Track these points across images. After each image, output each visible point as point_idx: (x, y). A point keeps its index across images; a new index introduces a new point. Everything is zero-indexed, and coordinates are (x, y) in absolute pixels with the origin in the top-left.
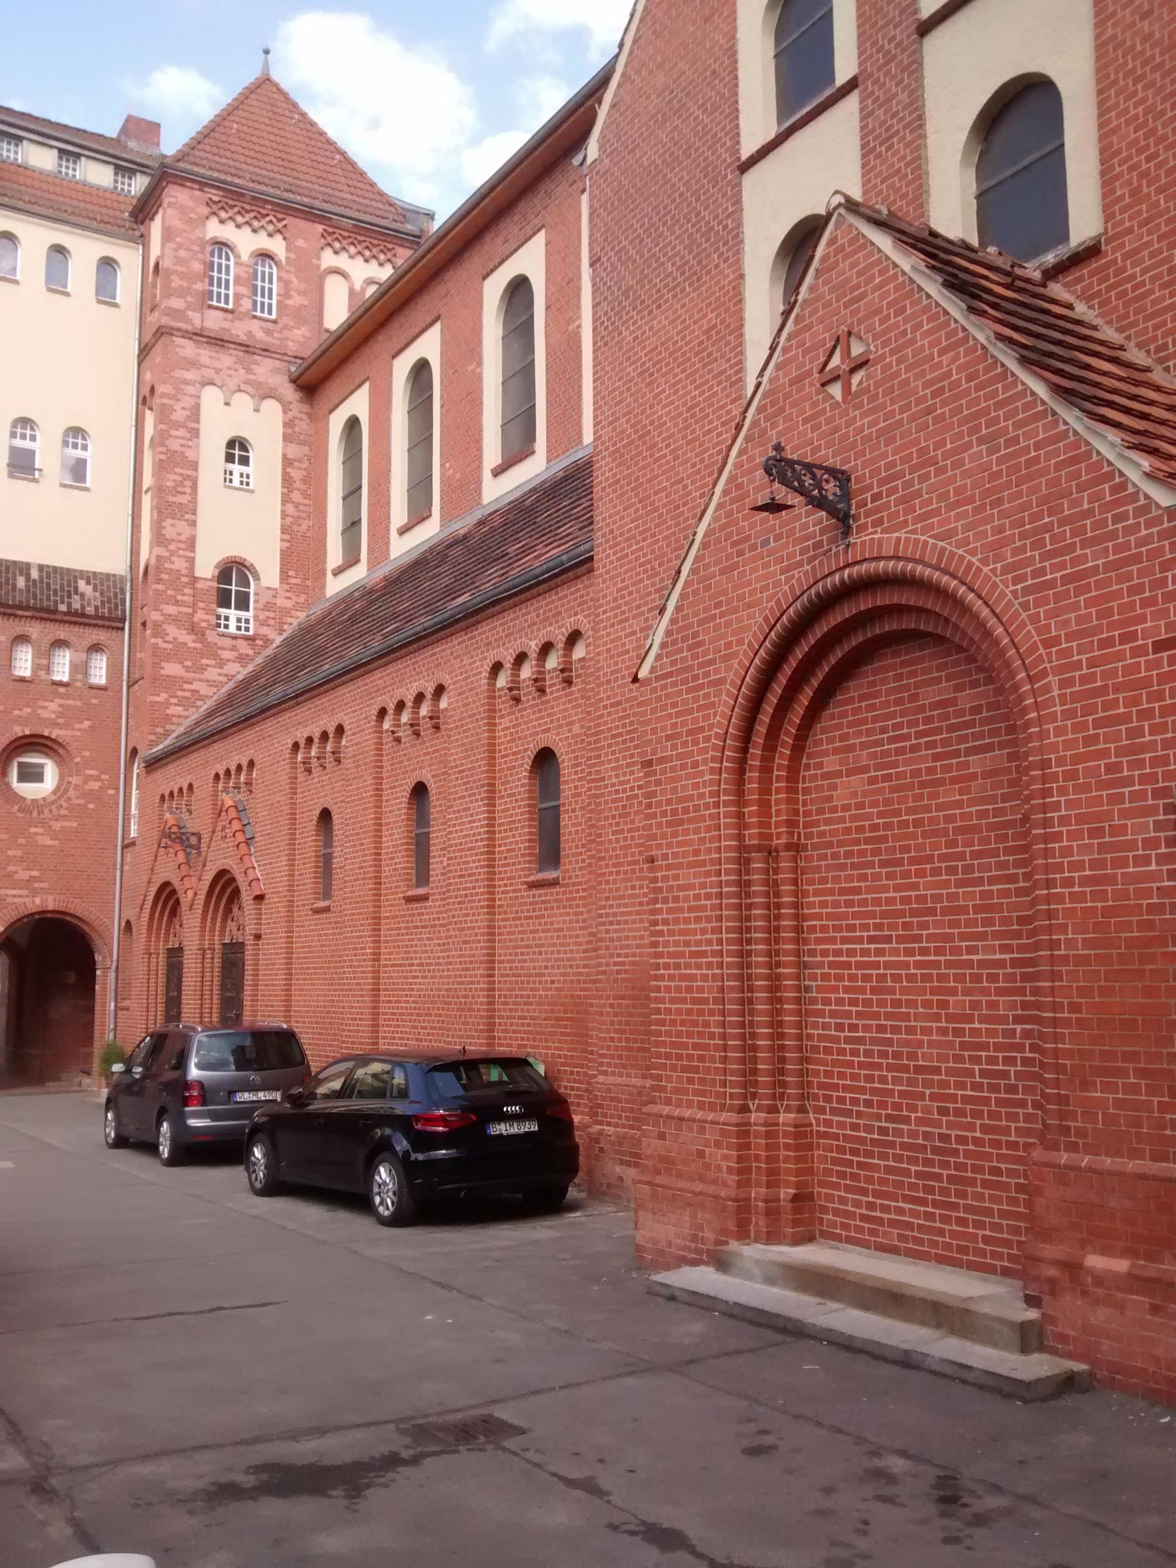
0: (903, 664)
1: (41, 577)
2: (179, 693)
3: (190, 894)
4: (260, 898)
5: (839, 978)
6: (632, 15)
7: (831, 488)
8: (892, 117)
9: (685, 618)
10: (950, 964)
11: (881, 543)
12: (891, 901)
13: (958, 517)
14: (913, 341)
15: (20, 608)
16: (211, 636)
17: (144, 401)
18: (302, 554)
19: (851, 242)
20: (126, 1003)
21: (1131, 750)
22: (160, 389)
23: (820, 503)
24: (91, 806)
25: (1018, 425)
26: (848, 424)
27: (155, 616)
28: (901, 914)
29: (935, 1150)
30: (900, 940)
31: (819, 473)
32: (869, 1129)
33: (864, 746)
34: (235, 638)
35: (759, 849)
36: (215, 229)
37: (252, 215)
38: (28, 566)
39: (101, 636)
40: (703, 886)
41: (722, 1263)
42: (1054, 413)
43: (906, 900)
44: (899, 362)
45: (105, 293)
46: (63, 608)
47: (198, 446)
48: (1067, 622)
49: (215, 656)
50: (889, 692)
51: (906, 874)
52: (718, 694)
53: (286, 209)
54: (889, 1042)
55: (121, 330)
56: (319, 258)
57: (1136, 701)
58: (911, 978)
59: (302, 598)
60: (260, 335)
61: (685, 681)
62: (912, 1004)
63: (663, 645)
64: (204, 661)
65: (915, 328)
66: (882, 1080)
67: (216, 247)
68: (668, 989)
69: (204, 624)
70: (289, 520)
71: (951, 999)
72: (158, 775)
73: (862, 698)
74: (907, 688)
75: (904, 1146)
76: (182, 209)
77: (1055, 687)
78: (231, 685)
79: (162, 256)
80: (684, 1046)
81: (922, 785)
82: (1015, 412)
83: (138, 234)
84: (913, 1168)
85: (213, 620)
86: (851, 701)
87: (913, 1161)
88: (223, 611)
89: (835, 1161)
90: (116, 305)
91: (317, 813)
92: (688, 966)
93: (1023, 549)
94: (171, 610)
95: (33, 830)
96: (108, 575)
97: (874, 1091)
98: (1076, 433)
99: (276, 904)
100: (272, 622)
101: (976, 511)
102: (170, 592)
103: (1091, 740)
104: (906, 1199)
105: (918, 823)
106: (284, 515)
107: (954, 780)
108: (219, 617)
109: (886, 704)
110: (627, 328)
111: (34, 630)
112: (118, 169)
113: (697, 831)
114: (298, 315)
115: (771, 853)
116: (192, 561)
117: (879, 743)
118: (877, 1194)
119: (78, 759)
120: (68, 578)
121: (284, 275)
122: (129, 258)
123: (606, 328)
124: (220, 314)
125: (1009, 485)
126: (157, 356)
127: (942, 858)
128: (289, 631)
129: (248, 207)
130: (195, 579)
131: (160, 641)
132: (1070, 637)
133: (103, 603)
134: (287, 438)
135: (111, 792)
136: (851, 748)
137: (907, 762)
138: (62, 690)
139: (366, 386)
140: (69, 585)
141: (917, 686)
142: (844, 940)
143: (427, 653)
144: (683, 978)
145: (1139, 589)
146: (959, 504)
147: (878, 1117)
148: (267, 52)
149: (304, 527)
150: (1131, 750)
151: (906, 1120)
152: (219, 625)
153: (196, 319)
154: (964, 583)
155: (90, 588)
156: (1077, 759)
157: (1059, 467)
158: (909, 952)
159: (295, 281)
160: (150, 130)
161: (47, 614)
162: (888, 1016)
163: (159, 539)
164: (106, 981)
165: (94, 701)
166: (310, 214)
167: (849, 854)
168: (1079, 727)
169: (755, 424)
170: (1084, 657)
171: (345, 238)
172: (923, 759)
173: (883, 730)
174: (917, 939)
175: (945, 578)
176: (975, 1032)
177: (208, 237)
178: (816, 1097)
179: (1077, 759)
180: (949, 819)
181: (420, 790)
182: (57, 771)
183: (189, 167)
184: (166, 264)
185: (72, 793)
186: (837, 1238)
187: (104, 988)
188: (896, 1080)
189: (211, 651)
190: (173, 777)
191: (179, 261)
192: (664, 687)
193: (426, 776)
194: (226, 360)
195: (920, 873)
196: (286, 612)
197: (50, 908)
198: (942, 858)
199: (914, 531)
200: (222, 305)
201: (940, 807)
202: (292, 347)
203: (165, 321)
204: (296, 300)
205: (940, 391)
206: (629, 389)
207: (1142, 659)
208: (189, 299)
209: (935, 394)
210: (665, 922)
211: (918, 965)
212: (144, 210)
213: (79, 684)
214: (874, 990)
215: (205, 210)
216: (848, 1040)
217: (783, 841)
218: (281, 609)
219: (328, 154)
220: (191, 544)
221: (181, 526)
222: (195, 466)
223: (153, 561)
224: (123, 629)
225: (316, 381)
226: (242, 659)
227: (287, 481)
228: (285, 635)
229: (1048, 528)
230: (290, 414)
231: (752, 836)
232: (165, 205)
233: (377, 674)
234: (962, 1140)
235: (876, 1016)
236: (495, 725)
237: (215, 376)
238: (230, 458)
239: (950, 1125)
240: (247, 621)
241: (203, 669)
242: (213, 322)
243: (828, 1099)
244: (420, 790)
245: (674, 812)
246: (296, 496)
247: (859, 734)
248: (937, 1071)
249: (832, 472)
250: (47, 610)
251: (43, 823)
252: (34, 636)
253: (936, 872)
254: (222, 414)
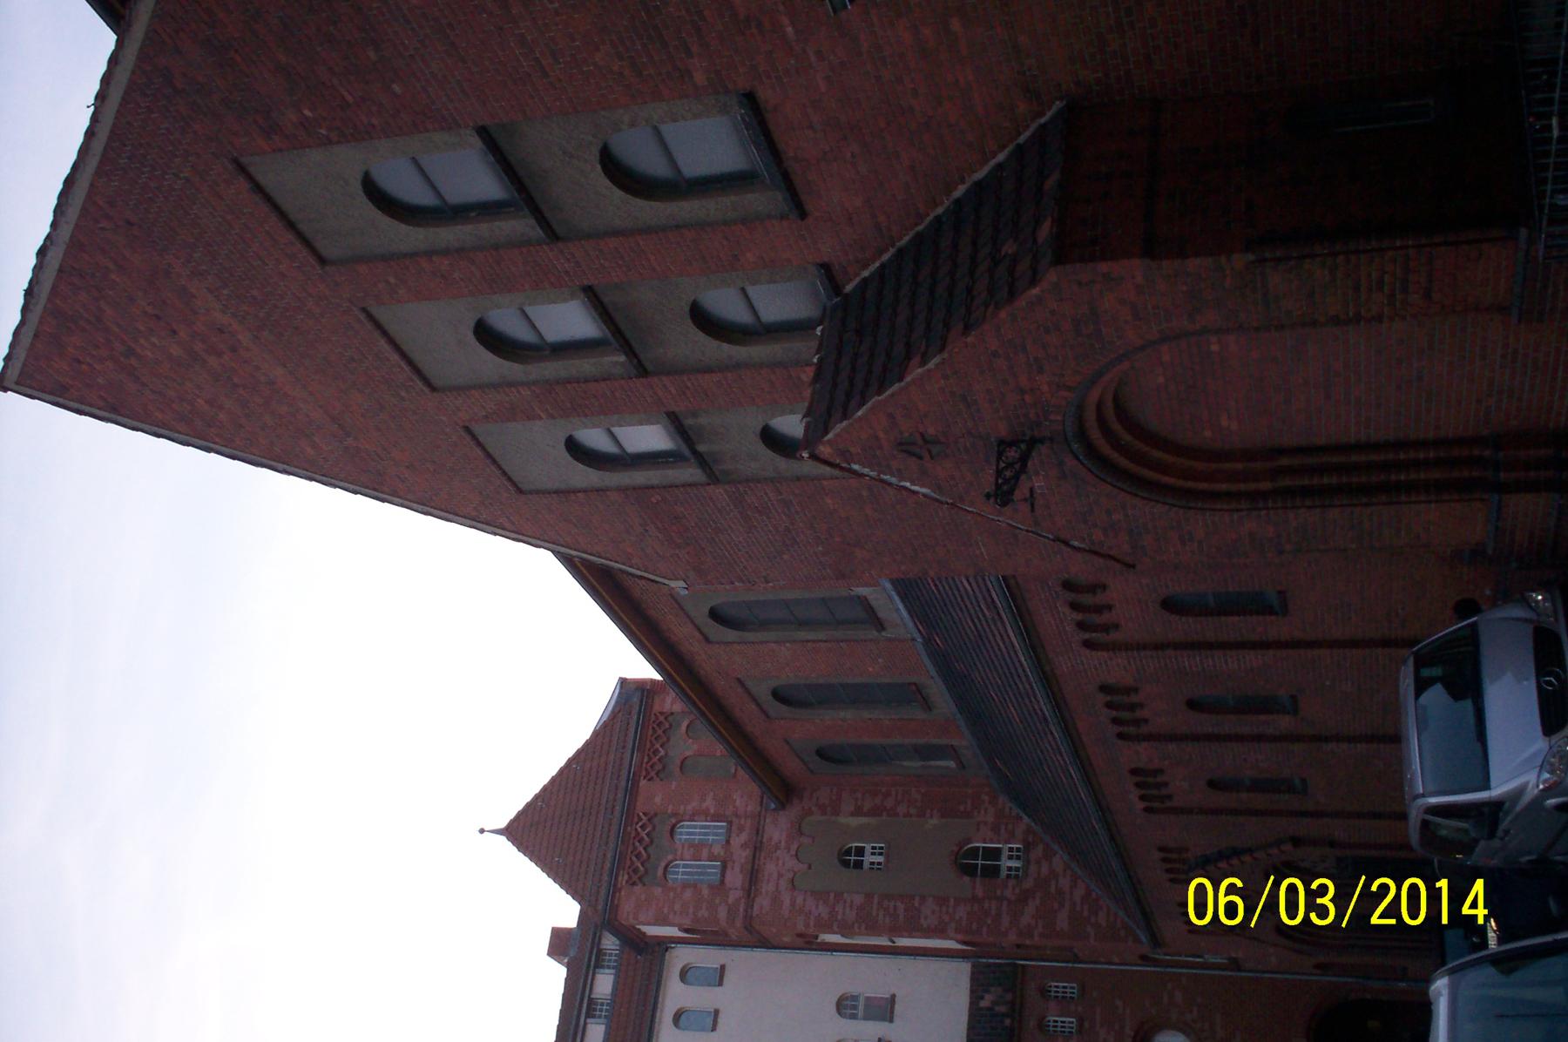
2: (1086, 913)
16: (1028, 884)
17: (808, 943)
22: (801, 927)
23: (1024, 459)
31: (1002, 465)
34: (1028, 862)
46: (1008, 1022)
55: (737, 960)
60: (744, 837)
64: (1053, 889)
85: (1012, 882)
88: (1004, 873)
94: (1006, 920)
108: (1008, 876)
112: (598, 965)
122: (682, 956)
128: (1016, 811)
138: (1086, 1025)
163: (940, 932)
202: (752, 807)
203: (739, 923)
223: (960, 937)
232: (632, 921)
240: (1011, 849)
242: (735, 879)
249: (1000, 454)
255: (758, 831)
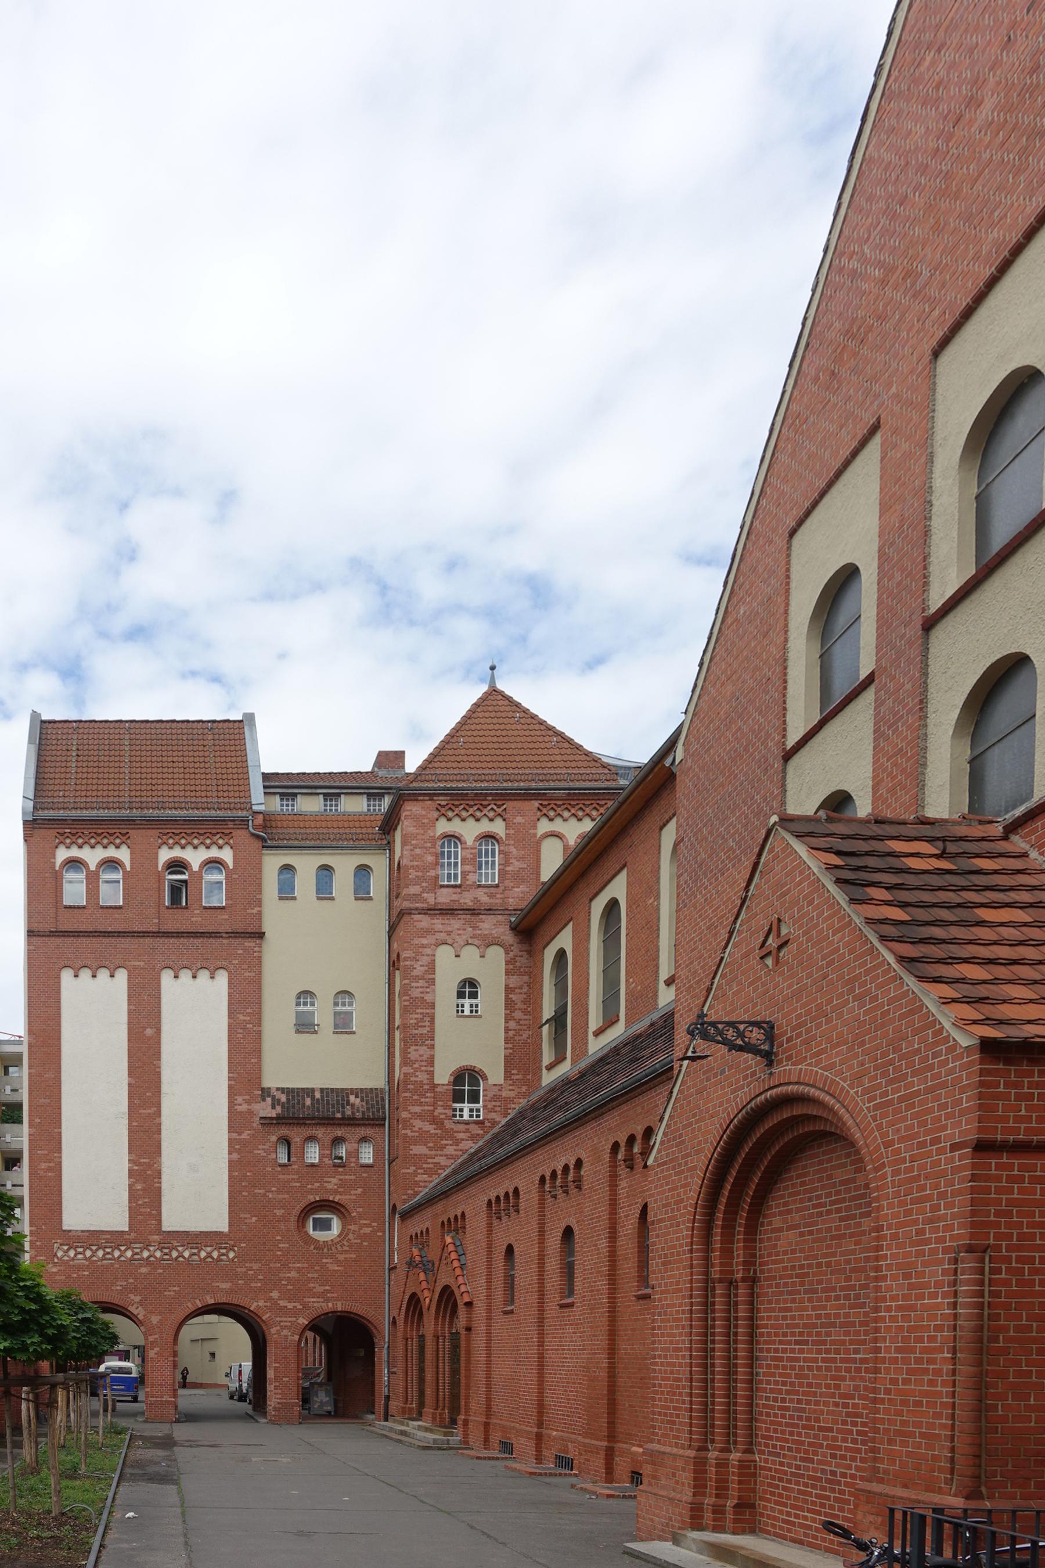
0: (825, 1153)
1: (322, 1097)
2: (425, 1166)
3: (427, 1300)
4: (469, 1304)
5: (777, 1367)
6: (709, 638)
7: (755, 1035)
8: (899, 704)
9: (675, 1123)
10: (842, 1360)
11: (796, 1073)
12: (809, 1317)
13: (837, 1054)
14: (817, 925)
15: (308, 1119)
16: (448, 1124)
17: (394, 964)
18: (521, 1058)
19: (783, 850)
20: (394, 1370)
21: (931, 1221)
22: (403, 955)
24: (365, 1244)
25: (879, 987)
26: (775, 987)
27: (404, 1115)
28: (815, 1326)
29: (828, 1481)
30: (814, 1343)
32: (790, 1466)
33: (798, 1210)
34: (467, 1123)
35: (721, 1281)
36: (443, 827)
37: (475, 808)
38: (313, 1090)
39: (368, 1131)
40: (681, 1305)
41: (676, 1541)
42: (901, 978)
43: (818, 1317)
44: (808, 941)
45: (362, 893)
47: (434, 991)
48: (898, 1130)
49: (452, 1137)
50: (815, 1172)
51: (819, 1299)
52: (692, 1177)
53: (503, 797)
54: (803, 1410)
55: (376, 914)
56: (535, 827)
57: (937, 1186)
58: (819, 1368)
59: (524, 1089)
60: (485, 899)
61: (674, 1168)
62: (819, 1386)
63: (662, 1143)
64: (444, 1142)
65: (819, 916)
66: (799, 1434)
67: (446, 840)
68: (660, 1371)
69: (442, 1116)
70: (511, 1033)
71: (842, 1383)
72: (409, 1222)
73: (798, 1177)
74: (825, 1170)
75: (810, 1477)
76: (417, 819)
77: (889, 1175)
78: (465, 1156)
79: (401, 857)
80: (668, 1407)
81: (832, 1238)
82: (877, 977)
83: (385, 842)
84: (814, 1491)
85: (450, 1113)
86: (791, 1178)
87: (814, 1487)
89: (770, 1485)
90: (370, 899)
91: (505, 1247)
92: (671, 1357)
93: (875, 1077)
94: (417, 1109)
95: (325, 1261)
96: (371, 1089)
97: (794, 1442)
98: (913, 992)
99: (480, 1307)
100: (498, 1109)
101: (849, 1050)
102: (415, 1097)
103: (908, 1213)
104: (809, 1511)
105: (828, 1264)
106: (507, 1030)
107: (852, 1235)
108: (455, 1110)
109: (812, 1182)
110: (701, 893)
111: (320, 1132)
113: (678, 1269)
114: (519, 878)
115: (731, 1284)
116: (431, 1074)
117: (807, 1208)
118: (793, 1507)
119: (354, 1214)
120: (342, 1095)
121: (506, 849)
122: (379, 863)
123: (686, 893)
124: (451, 890)
125: (869, 1031)
126: (400, 932)
127: (842, 1289)
129: (472, 803)
130: (435, 1086)
131: (408, 1132)
132: (901, 1140)
133: (368, 1109)
134: (508, 973)
135: (380, 1234)
136: (789, 1212)
137: (824, 1222)
139: (570, 927)
140: (343, 1100)
141: (833, 1168)
142: (781, 1342)
143: (570, 1136)
144: (669, 1364)
145: (945, 1106)
146: (838, 1045)
147: (795, 1458)
148: (493, 668)
149: (525, 1036)
150: (931, 1221)
151: (812, 1461)
152: (455, 1116)
153: (430, 898)
154: (839, 1102)
155: (358, 1100)
156: (900, 1225)
157: (902, 1017)
158: (819, 1352)
159: (514, 851)
160: (396, 758)
161: (328, 1121)
162: (804, 1393)
163: (406, 1062)
164: (382, 1355)
165: (364, 1175)
166: (527, 795)
167: (786, 1285)
168: (902, 1204)
169: (719, 987)
170: (908, 1154)
171: (559, 806)
172: (833, 1220)
173: (810, 1199)
174: (824, 1343)
175: (828, 1098)
176: (855, 1406)
177: (438, 834)
178: (760, 1444)
179: (900, 1225)
180: (848, 1262)
181: (568, 1232)
182: (340, 1223)
183: (421, 785)
184: (404, 862)
185: (351, 1236)
186: (768, 1532)
187: (380, 1359)
188: (807, 1435)
189: (449, 1134)
190: (419, 1224)
191: (414, 858)
192: (662, 1171)
193: (572, 1222)
194: (455, 924)
195: (828, 1299)
196: (511, 1100)
197: (339, 1309)
198: (842, 1289)
199: (810, 1065)
200: (452, 883)
201: (842, 1254)
202: (512, 903)
203: (406, 904)
204: (516, 865)
205: (832, 962)
206: (700, 940)
207: (942, 1157)
208: (424, 884)
209: (828, 965)
210: (660, 1328)
211: (824, 1360)
212: (389, 824)
213: (353, 1165)
214: (797, 1376)
215: (436, 814)
216: (780, 1408)
217: (740, 1275)
218: (506, 1099)
219: (547, 739)
220: (431, 1061)
221: (423, 1050)
222: (432, 1006)
224: (384, 1125)
225: (530, 928)
226: (474, 1138)
227: (509, 1004)
228: (509, 1117)
229: (891, 1062)
230: (511, 954)
231: (715, 1272)
232: (403, 818)
233: (539, 1152)
234: (843, 1475)
235: (797, 1393)
236: (617, 1186)
237: (447, 938)
238: (461, 995)
239: (837, 1465)
240: (478, 1110)
241: (444, 1147)
242: (444, 897)
243: (767, 1445)
244: (568, 1232)
245: (666, 1255)
246: (518, 1015)
247: (795, 1201)
248: (831, 1430)
250: (328, 1119)
251: (331, 1256)
252: (320, 1136)
253: (837, 1298)
254: (451, 966)
255: (490, 911)
